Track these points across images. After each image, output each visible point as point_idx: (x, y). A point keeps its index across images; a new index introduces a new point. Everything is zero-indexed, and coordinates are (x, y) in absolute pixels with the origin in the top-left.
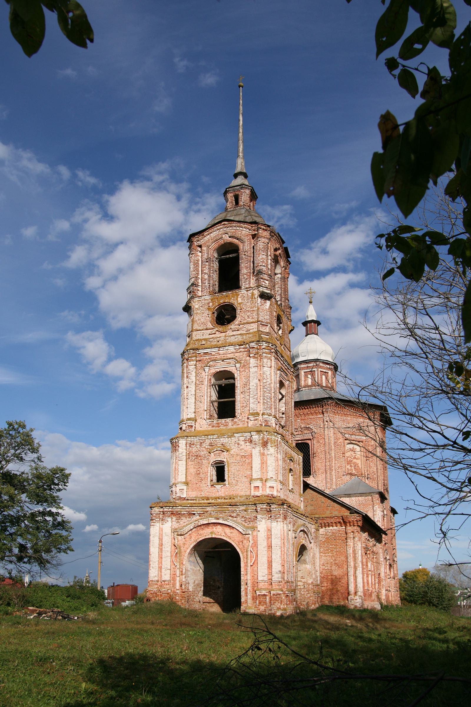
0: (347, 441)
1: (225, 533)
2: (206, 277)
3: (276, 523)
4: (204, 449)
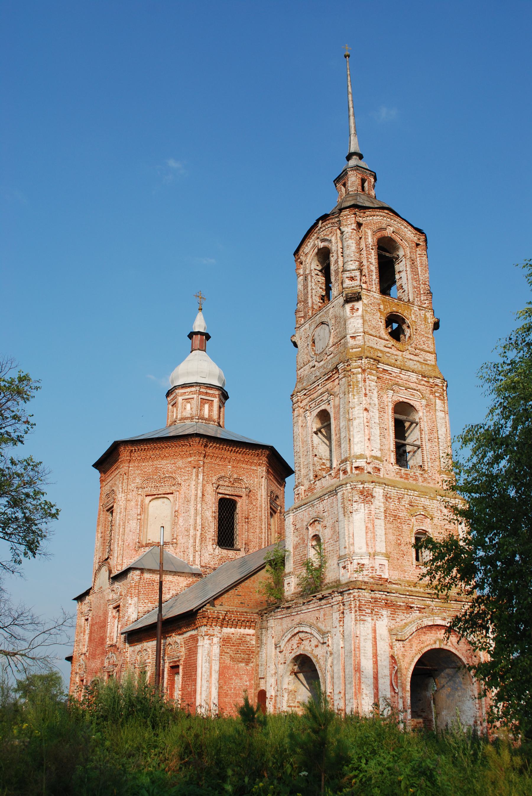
4: (403, 508)
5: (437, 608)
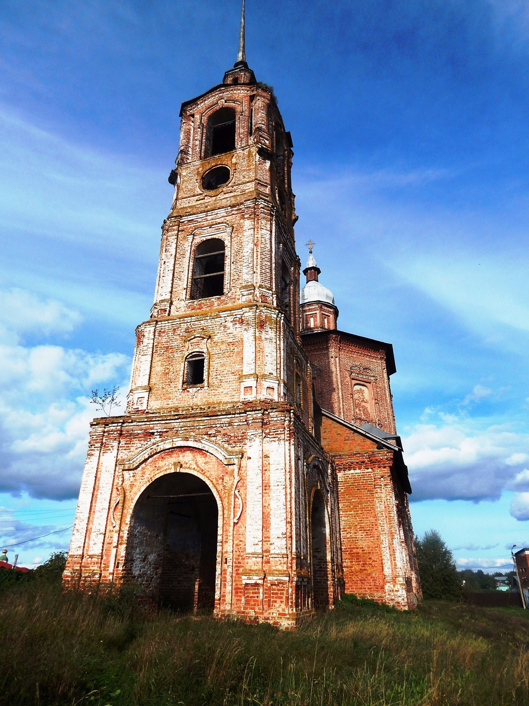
0: (354, 382)
1: (196, 463)
2: (197, 143)
3: (277, 442)
4: (178, 337)
5: (183, 429)
